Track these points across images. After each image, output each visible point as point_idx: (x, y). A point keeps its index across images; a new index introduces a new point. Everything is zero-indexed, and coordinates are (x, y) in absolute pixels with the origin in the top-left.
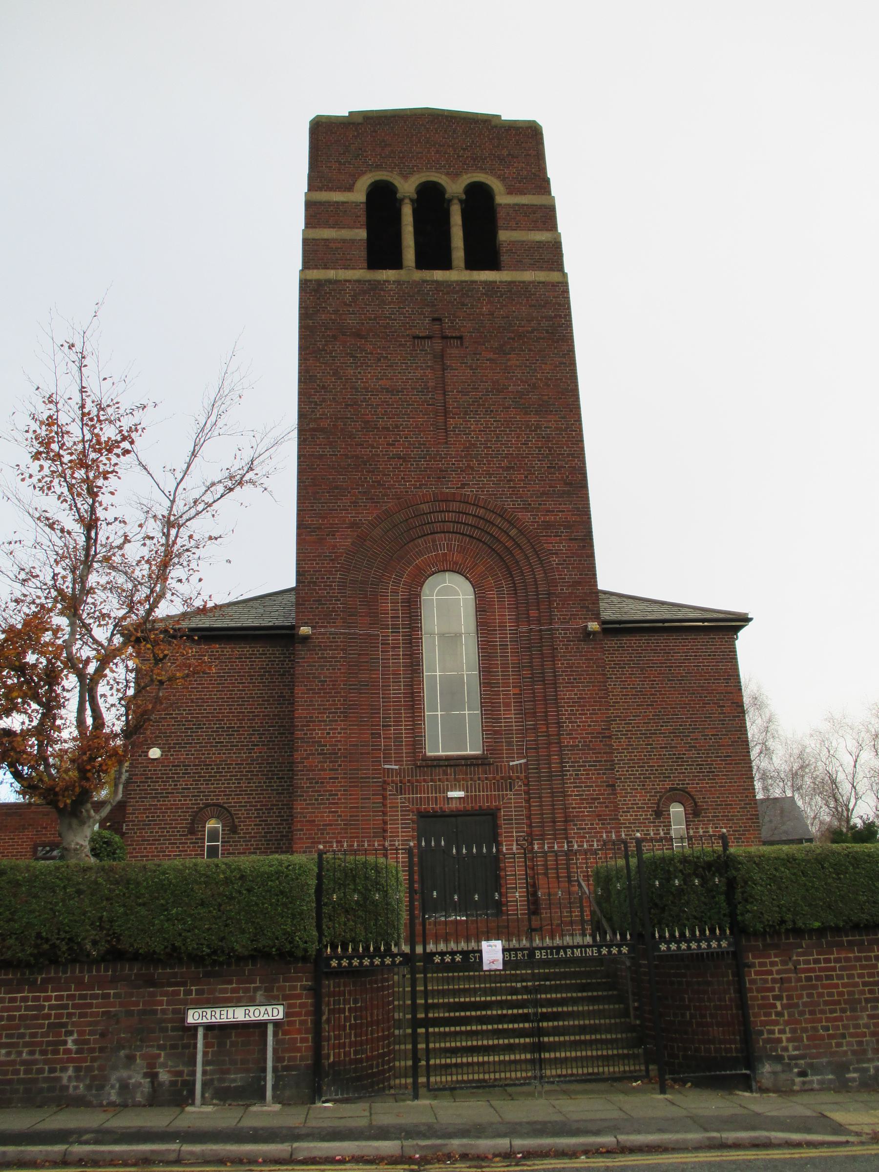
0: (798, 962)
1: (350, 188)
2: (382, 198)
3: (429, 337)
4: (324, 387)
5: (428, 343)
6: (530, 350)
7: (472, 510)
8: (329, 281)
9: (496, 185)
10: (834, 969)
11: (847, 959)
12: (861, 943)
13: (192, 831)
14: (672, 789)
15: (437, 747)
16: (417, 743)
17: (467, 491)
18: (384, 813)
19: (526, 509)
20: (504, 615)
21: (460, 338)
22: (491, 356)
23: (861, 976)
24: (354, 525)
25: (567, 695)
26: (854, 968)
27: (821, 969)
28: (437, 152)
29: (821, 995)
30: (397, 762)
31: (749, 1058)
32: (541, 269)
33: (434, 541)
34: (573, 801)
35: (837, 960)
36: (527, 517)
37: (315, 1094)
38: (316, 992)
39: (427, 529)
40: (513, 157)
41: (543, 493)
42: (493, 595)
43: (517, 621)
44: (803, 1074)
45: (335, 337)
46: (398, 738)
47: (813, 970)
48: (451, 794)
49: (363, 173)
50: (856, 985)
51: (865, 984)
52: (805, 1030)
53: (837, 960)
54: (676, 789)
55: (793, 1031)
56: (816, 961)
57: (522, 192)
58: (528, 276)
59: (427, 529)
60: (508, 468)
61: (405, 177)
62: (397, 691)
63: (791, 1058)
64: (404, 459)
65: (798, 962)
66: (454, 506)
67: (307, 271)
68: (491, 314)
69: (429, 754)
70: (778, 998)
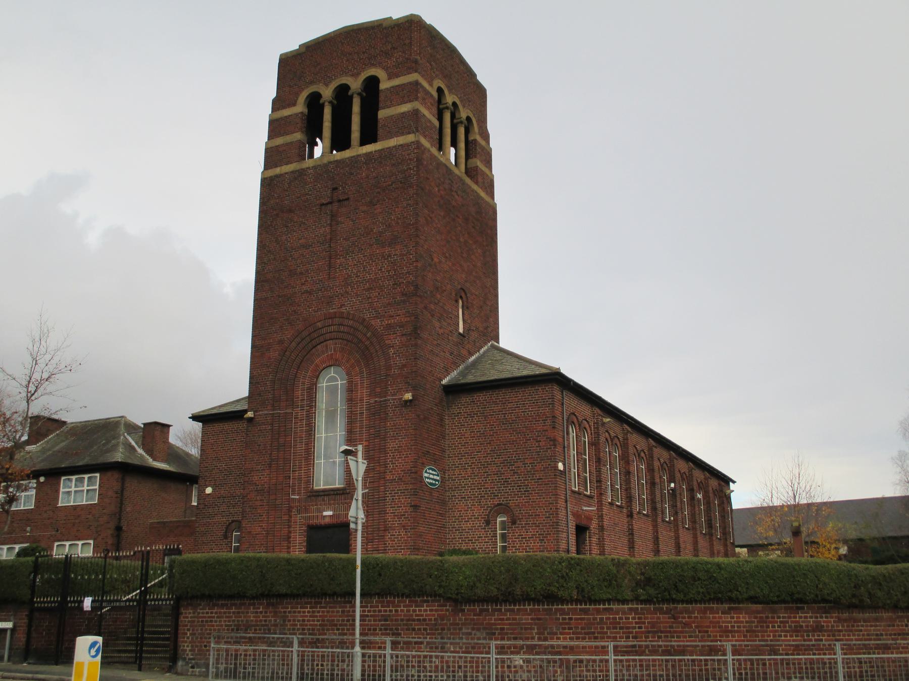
0: (199, 613)
1: (294, 104)
2: (314, 101)
3: (330, 203)
4: (269, 251)
5: (329, 206)
6: (389, 199)
7: (346, 322)
8: (277, 176)
9: (381, 74)
10: (213, 617)
11: (220, 613)
12: (227, 605)
13: (226, 537)
14: (499, 505)
15: (321, 482)
16: (309, 479)
17: (343, 310)
18: (289, 527)
19: (376, 317)
20: (363, 392)
21: (348, 199)
22: (365, 208)
23: (225, 621)
24: (281, 342)
25: (391, 445)
26: (222, 617)
27: (209, 617)
28: (348, 60)
29: (206, 630)
30: (299, 494)
31: (174, 659)
32: (403, 134)
33: (327, 346)
34: (389, 517)
35: (216, 613)
36: (376, 323)
37: (25, 659)
38: (30, 618)
39: (322, 339)
40: (394, 48)
41: (389, 304)
42: (357, 379)
43: (370, 395)
44: (193, 667)
45: (277, 215)
46: (300, 479)
47: (205, 617)
48: (325, 513)
49: (303, 90)
50: (222, 626)
51: (226, 626)
52: (197, 646)
53: (216, 613)
54: (501, 504)
55: (192, 646)
56: (207, 613)
57: (397, 76)
58: (393, 142)
59: (322, 339)
60: (368, 289)
61: (327, 85)
62: (301, 448)
63: (190, 659)
64: (310, 293)
65: (199, 613)
66: (337, 321)
67: (266, 172)
68: (367, 177)
69: (315, 488)
70: (188, 630)
